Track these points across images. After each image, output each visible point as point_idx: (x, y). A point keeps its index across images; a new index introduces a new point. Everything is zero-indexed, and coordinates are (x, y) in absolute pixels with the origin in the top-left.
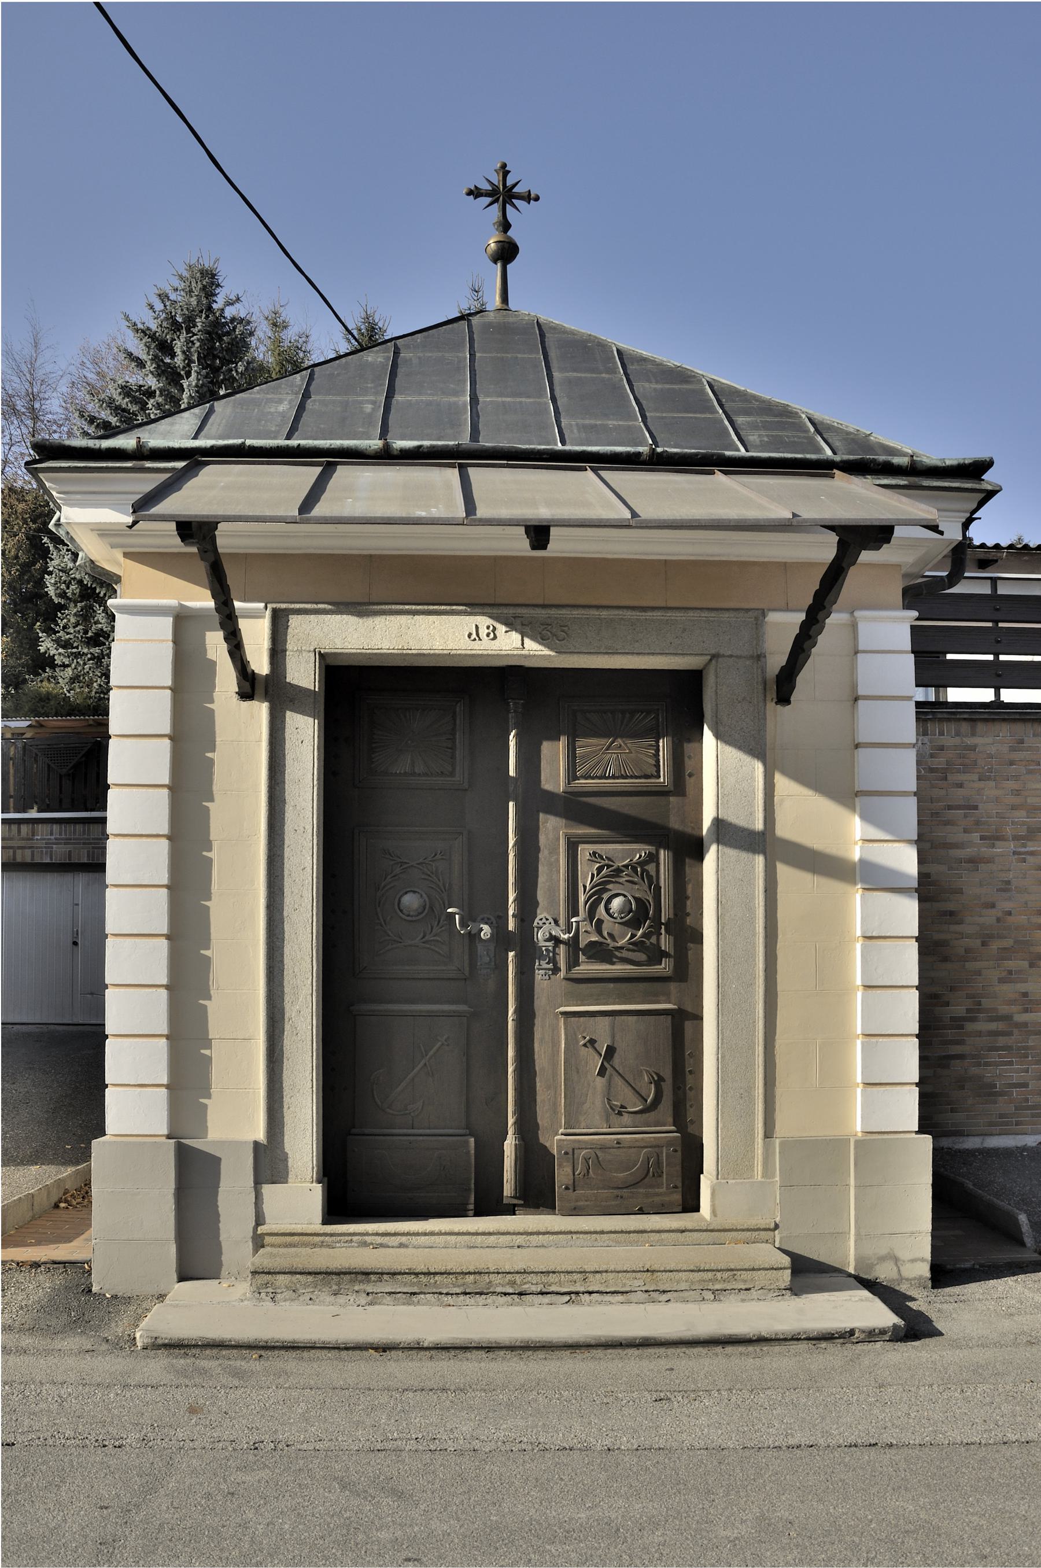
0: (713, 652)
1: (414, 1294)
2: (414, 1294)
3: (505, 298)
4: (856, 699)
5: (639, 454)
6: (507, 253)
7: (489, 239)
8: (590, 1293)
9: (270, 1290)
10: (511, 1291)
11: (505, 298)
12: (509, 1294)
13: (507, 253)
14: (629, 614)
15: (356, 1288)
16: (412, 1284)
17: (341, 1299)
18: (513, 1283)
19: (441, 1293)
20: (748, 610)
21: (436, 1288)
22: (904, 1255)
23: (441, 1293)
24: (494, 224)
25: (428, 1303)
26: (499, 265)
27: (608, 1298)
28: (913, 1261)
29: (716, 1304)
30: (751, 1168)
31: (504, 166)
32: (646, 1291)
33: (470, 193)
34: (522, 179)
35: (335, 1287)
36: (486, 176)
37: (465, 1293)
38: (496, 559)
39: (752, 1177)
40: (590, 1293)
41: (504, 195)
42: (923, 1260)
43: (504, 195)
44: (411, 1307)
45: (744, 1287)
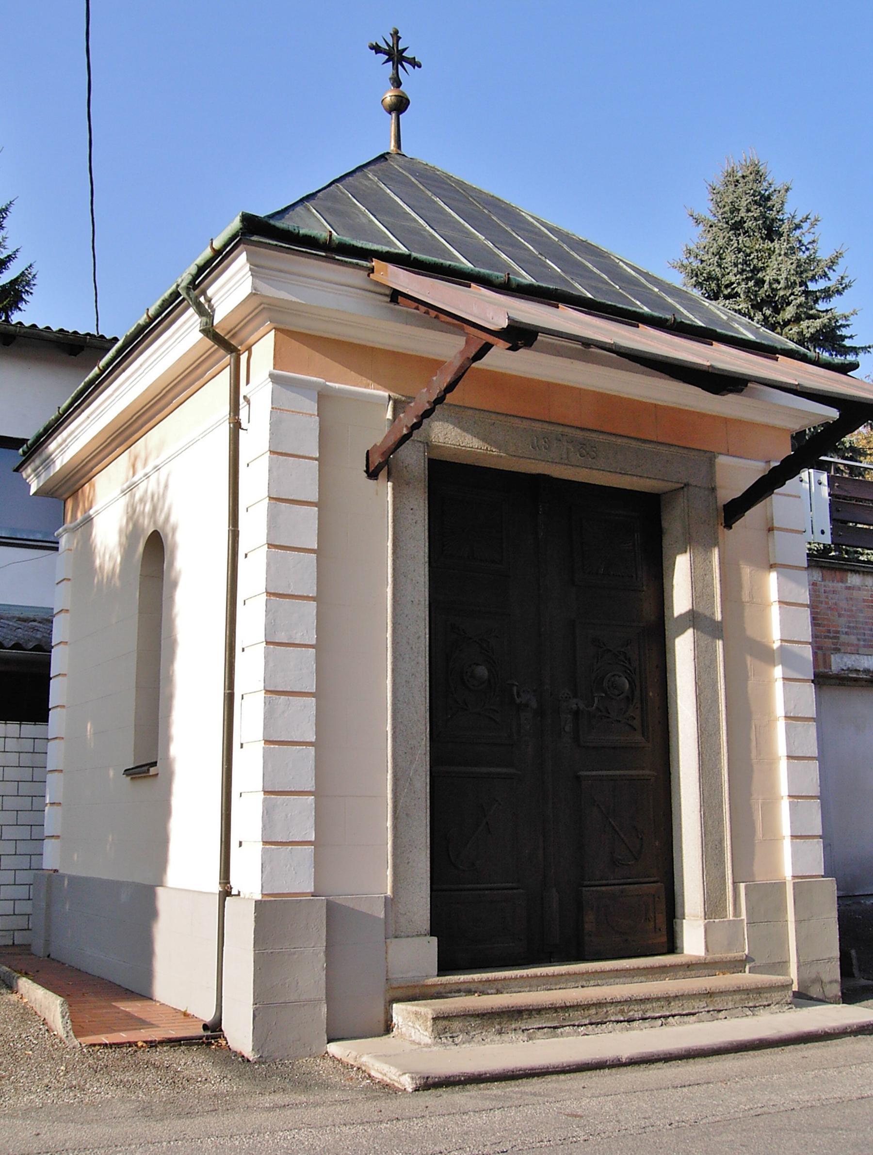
0: (685, 481)
1: (555, 1028)
2: (555, 1028)
3: (399, 146)
4: (771, 529)
5: (667, 320)
6: (400, 106)
7: (385, 93)
8: (673, 1016)
9: (448, 1035)
10: (622, 1019)
11: (399, 146)
12: (621, 1022)
13: (400, 106)
14: (634, 444)
15: (513, 1026)
16: (553, 1019)
17: (505, 1037)
18: (622, 1012)
19: (574, 1026)
20: (706, 452)
21: (571, 1021)
22: (826, 978)
23: (574, 1026)
24: (390, 79)
25: (569, 1035)
26: (394, 115)
27: (686, 1019)
28: (831, 982)
29: (755, 1018)
30: (725, 908)
31: (396, 32)
32: (708, 1011)
33: (372, 48)
34: (411, 47)
35: (497, 1027)
36: (383, 38)
37: (591, 1024)
38: (549, 384)
39: (726, 917)
40: (673, 1016)
41: (396, 56)
42: (836, 981)
43: (396, 56)
44: (556, 1039)
45: (766, 1003)
